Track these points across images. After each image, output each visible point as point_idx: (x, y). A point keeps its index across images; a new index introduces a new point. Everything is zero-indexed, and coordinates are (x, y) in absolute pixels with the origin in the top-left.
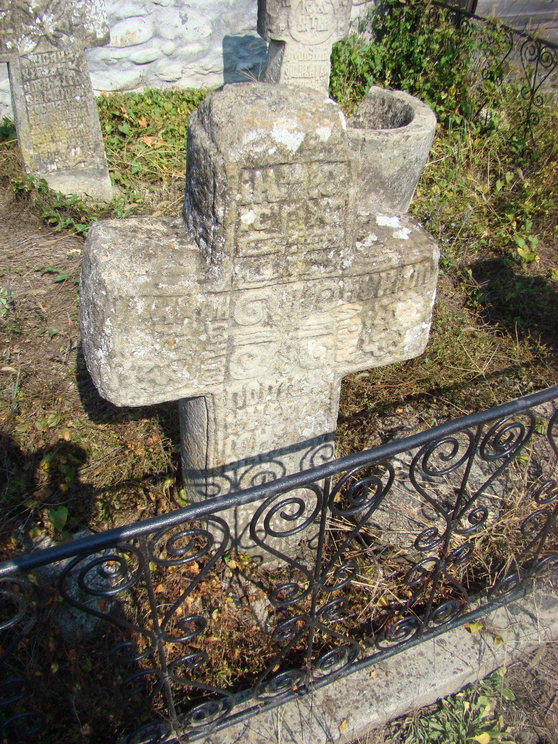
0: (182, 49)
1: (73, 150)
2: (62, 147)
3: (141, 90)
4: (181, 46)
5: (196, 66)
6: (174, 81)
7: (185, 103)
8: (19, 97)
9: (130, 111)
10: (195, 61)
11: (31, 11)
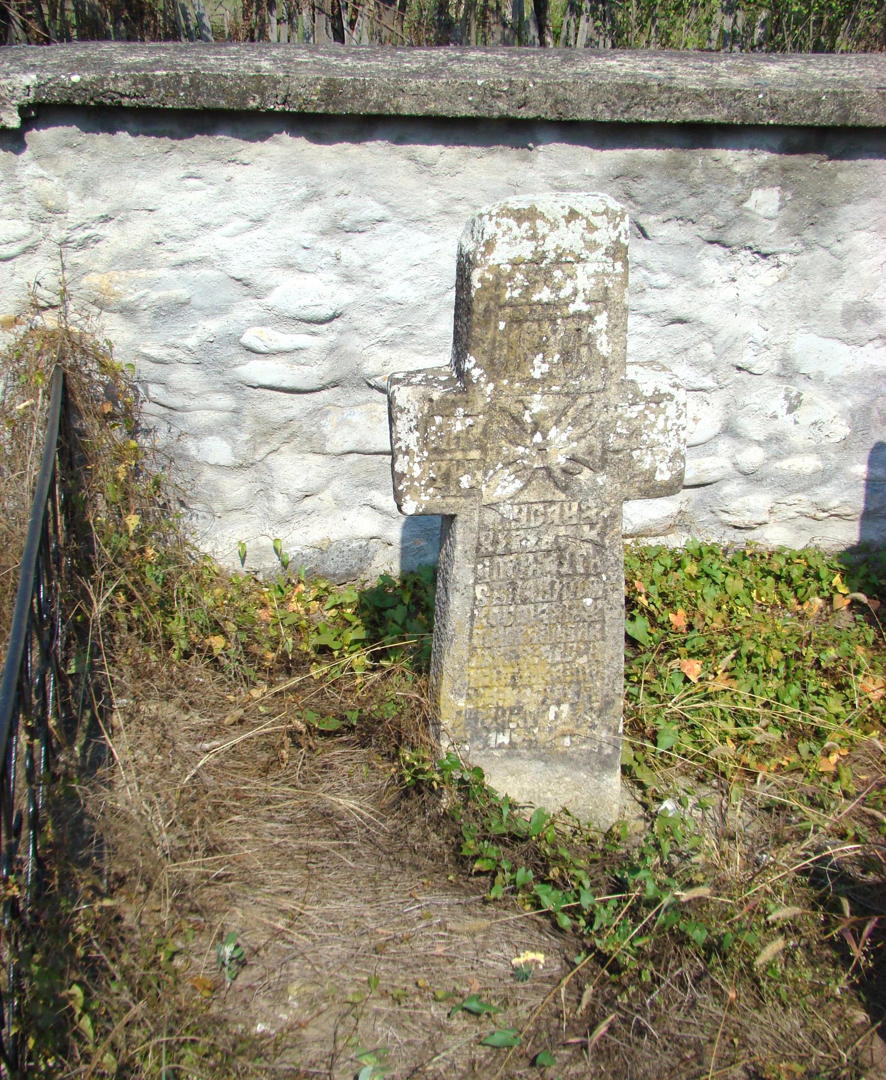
0: (778, 464)
1: (553, 709)
2: (530, 699)
3: (677, 541)
4: (778, 457)
5: (803, 501)
6: (749, 528)
7: (770, 580)
8: (460, 586)
9: (653, 589)
10: (803, 490)
11: (527, 418)
